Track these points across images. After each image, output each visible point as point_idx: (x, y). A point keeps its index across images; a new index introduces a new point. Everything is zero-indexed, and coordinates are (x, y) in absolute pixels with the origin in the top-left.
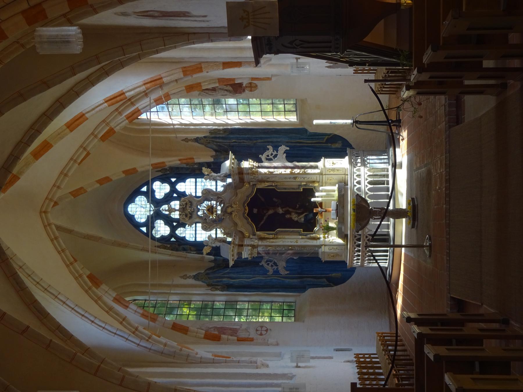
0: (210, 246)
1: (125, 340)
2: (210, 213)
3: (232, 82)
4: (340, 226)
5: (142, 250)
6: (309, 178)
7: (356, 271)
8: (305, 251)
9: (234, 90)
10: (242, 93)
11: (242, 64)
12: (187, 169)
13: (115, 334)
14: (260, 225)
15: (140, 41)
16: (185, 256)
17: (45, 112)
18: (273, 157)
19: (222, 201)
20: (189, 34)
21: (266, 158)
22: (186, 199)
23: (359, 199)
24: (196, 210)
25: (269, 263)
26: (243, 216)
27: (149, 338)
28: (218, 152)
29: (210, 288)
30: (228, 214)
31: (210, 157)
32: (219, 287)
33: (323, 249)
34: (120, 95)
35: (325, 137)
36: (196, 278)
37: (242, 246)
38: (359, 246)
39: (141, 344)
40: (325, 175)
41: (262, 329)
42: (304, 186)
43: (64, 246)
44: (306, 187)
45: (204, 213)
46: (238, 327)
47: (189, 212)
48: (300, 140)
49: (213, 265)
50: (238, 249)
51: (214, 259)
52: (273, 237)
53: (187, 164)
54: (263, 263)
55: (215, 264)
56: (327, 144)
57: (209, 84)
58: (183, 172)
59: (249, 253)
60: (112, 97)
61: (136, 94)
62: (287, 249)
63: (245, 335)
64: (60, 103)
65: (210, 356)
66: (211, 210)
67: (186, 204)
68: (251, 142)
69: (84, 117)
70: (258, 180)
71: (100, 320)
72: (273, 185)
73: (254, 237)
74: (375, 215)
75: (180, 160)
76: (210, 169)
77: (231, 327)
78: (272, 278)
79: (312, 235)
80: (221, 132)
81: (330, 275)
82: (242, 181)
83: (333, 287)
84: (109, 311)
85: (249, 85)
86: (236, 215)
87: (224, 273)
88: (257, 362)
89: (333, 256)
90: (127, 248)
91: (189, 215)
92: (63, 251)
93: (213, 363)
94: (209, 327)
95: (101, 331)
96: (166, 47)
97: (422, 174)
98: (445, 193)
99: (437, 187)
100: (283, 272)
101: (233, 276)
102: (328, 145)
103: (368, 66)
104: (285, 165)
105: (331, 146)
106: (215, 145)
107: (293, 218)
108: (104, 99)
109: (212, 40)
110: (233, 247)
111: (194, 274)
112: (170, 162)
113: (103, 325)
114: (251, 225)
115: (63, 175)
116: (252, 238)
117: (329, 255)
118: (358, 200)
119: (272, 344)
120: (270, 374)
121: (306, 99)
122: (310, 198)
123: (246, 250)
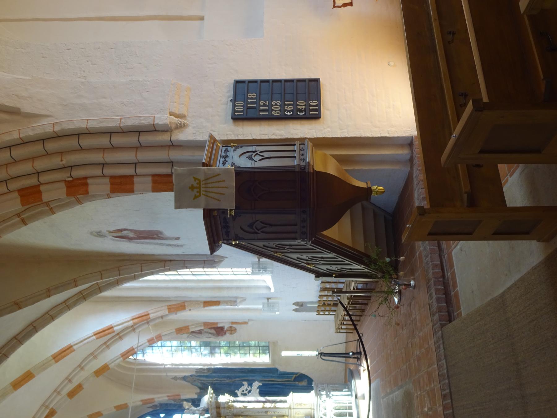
3: (215, 326)
6: (279, 412)
12: (175, 405)
20: (165, 261)
40: (293, 409)
53: (175, 400)
57: (196, 327)
60: (101, 331)
61: (124, 328)
64: (33, 326)
69: (71, 349)
70: (233, 414)
75: (168, 396)
80: (206, 371)
85: (230, 329)
96: (143, 272)
97: (395, 399)
98: (444, 413)
99: (426, 409)
103: (335, 278)
104: (257, 399)
105: (298, 384)
106: (199, 383)
108: (93, 333)
112: (159, 398)
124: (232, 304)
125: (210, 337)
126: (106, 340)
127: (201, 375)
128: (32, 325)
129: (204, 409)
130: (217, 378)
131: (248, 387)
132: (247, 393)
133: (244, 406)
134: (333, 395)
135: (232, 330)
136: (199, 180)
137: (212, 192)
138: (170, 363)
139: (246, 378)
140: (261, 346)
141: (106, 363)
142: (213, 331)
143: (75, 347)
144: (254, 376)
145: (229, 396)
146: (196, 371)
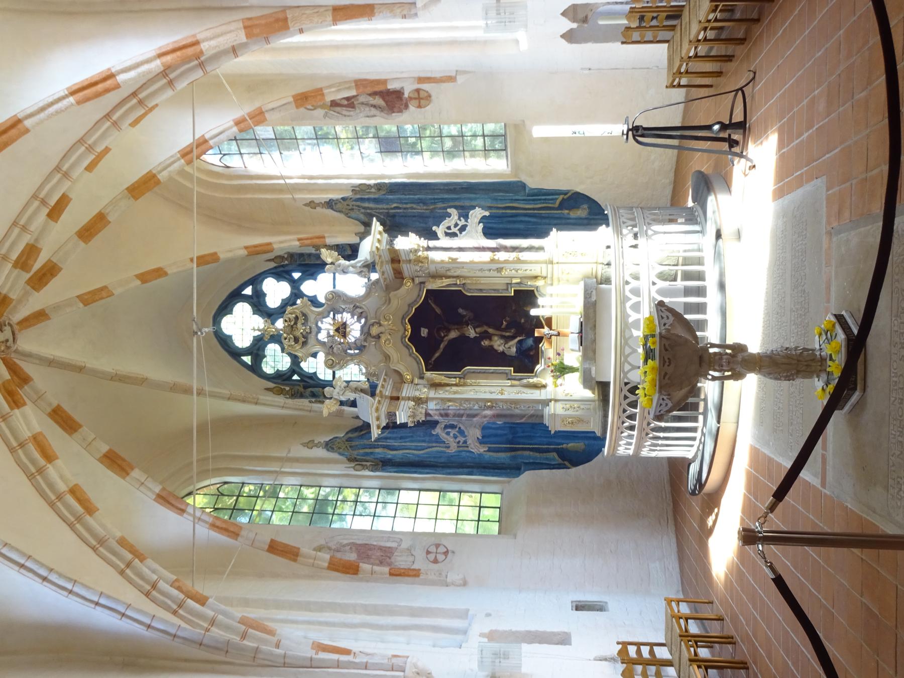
0: (336, 399)
3: (378, 88)
4: (587, 366)
5: (229, 399)
6: (526, 270)
8: (517, 411)
9: (387, 105)
10: (404, 111)
11: (376, 10)
13: (97, 604)
14: (433, 359)
16: (309, 409)
18: (459, 230)
19: (361, 313)
22: (295, 308)
23: (668, 318)
24: (314, 330)
26: (402, 343)
27: (180, 606)
29: (353, 465)
30: (374, 337)
32: (368, 464)
33: (552, 409)
34: (105, 79)
35: (557, 197)
37: (397, 398)
38: (632, 417)
40: (558, 263)
41: (437, 549)
42: (516, 285)
44: (520, 287)
45: (329, 336)
46: (394, 545)
47: (301, 333)
48: (512, 203)
52: (457, 381)
57: (339, 91)
58: (312, 263)
62: (483, 406)
63: (406, 561)
66: (342, 330)
67: (297, 318)
68: (425, 207)
69: (20, 126)
71: (60, 575)
72: (458, 283)
73: (421, 381)
74: (717, 368)
75: (299, 240)
77: (383, 544)
79: (531, 380)
80: (373, 190)
81: (564, 446)
82: (399, 275)
83: (569, 468)
84: (98, 546)
85: (416, 95)
86: (388, 339)
89: (572, 423)
91: (302, 340)
93: (311, 667)
94: (341, 543)
95: (64, 598)
102: (563, 212)
105: (569, 214)
106: (362, 213)
107: (496, 347)
108: (67, 89)
110: (379, 402)
111: (327, 439)
112: (281, 242)
113: (69, 586)
114: (415, 359)
116: (417, 384)
117: (563, 421)
118: (665, 320)
119: (453, 584)
121: (524, 121)
122: (528, 309)
123: (405, 408)
125: (375, 116)
126: (110, 109)
127: (363, 197)
129: (366, 264)
130: (397, 203)
132: (458, 232)
133: (450, 258)
134: (656, 233)
135: (421, 98)
138: (300, 174)
139: (457, 203)
140: (487, 136)
141: (150, 171)
142: (379, 101)
143: (28, 123)
144: (475, 199)
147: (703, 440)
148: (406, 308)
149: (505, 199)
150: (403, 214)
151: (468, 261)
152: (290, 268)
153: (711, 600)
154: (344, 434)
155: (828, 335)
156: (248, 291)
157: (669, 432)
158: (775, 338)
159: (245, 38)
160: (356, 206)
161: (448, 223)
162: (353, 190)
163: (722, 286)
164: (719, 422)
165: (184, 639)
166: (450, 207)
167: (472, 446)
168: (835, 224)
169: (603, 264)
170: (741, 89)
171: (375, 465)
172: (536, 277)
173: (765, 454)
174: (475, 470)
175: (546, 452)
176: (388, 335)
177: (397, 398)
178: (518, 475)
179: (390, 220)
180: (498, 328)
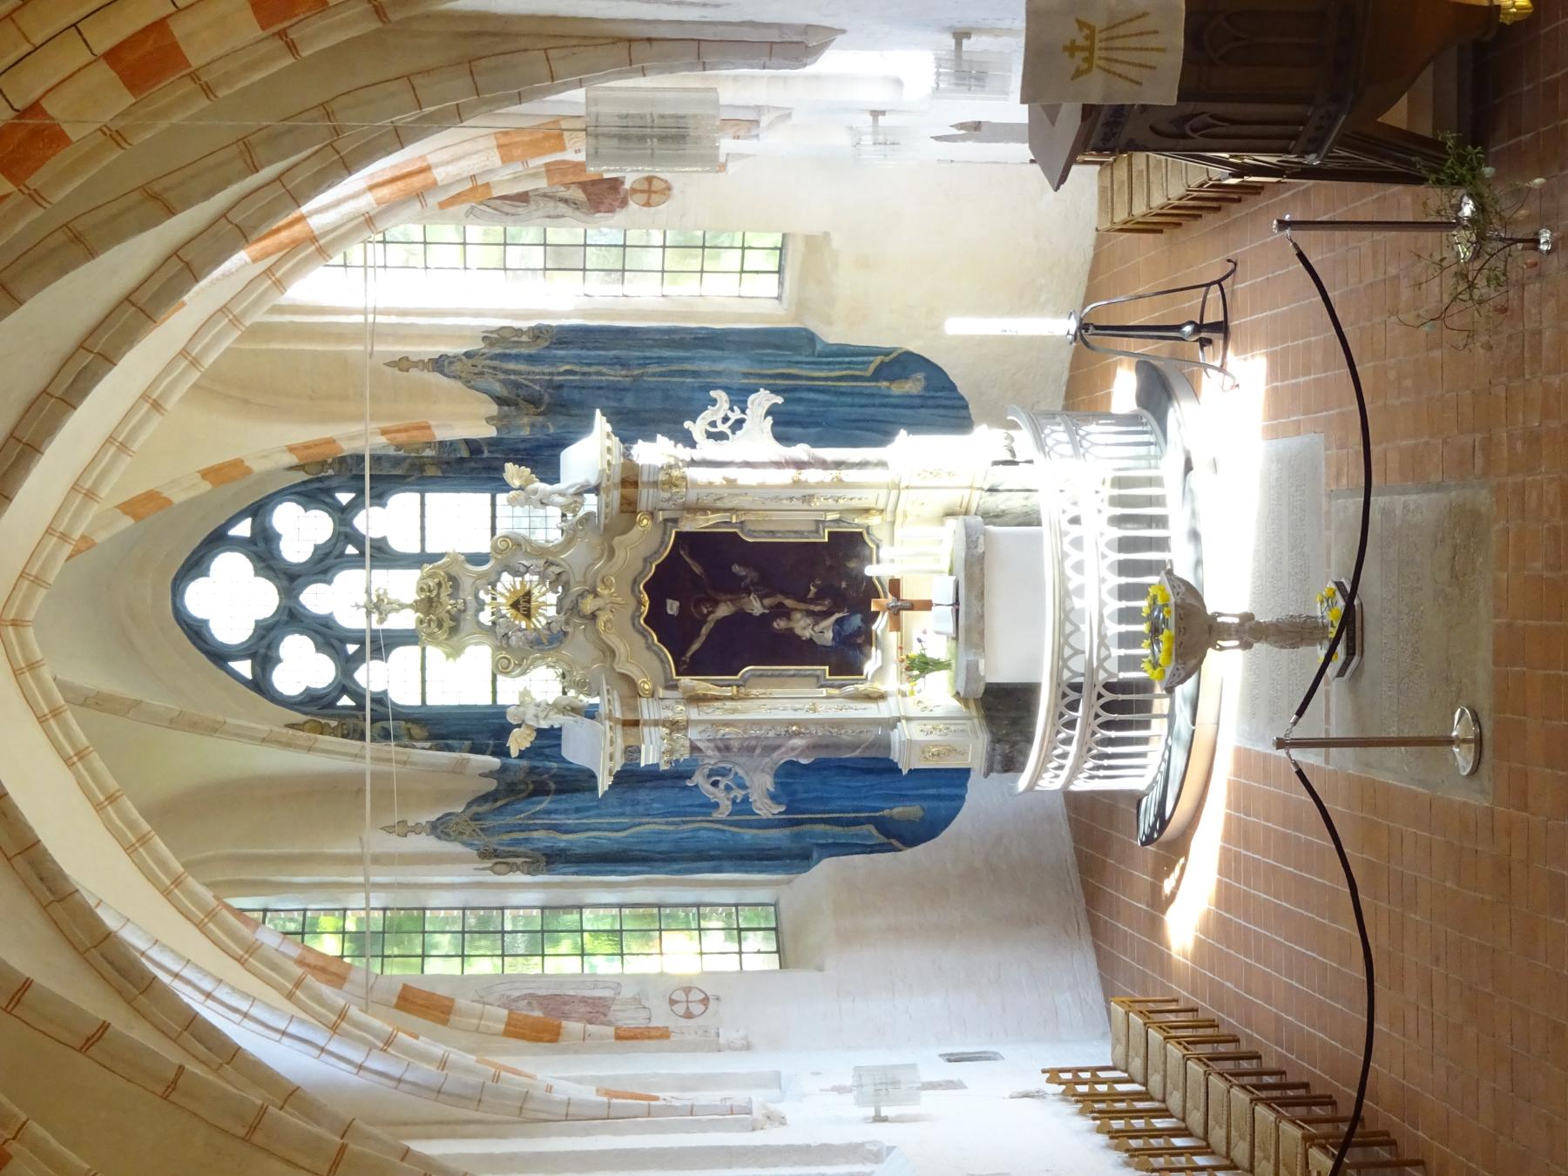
0: (529, 726)
1: (317, 1053)
2: (520, 616)
5: (263, 740)
6: (851, 499)
7: (967, 797)
9: (589, 200)
12: (397, 461)
13: (284, 1033)
14: (689, 654)
15: (470, 62)
17: (130, 294)
19: (559, 574)
21: (707, 432)
22: (438, 567)
25: (719, 778)
26: (634, 625)
28: (508, 405)
29: (490, 865)
30: (584, 617)
31: (484, 422)
32: (519, 861)
35: (871, 358)
36: (439, 831)
37: (636, 723)
39: (369, 1064)
40: (907, 488)
41: (687, 995)
42: (831, 524)
43: (83, 740)
46: (608, 993)
47: (448, 612)
48: (789, 367)
49: (491, 785)
50: (625, 734)
51: (499, 765)
52: (735, 692)
53: (399, 448)
54: (698, 779)
55: (499, 782)
56: (878, 381)
59: (663, 750)
62: (783, 733)
63: (634, 1018)
64: (182, 260)
65: (588, 1094)
66: (524, 604)
67: (439, 585)
68: (623, 373)
70: (684, 503)
72: (734, 521)
73: (669, 694)
75: (384, 432)
76: (529, 470)
77: (587, 993)
78: (697, 825)
80: (524, 338)
81: (886, 812)
82: (629, 507)
83: (900, 850)
84: (246, 956)
85: (646, 187)
87: (533, 814)
88: (751, 1109)
89: (939, 755)
90: (217, 735)
91: (448, 623)
92: (81, 755)
93: (608, 1118)
94: (508, 997)
100: (766, 809)
101: (563, 822)
102: (879, 384)
105: (889, 388)
106: (499, 380)
107: (798, 631)
109: (704, 63)
111: (433, 818)
112: (352, 438)
113: (244, 1006)
115: (81, 496)
117: (923, 752)
118: (1177, 590)
119: (731, 1047)
120: (808, 1146)
121: (827, 234)
124: (742, 133)
127: (508, 351)
128: (178, 257)
131: (731, 409)
132: (729, 432)
136: (1092, 29)
137: (1122, 62)
144: (722, 359)
145: (672, 443)
146: (484, 338)
147: (1166, 756)
148: (639, 565)
149: (776, 362)
150: (577, 384)
151: (755, 484)
152: (334, 483)
153: (1175, 997)
154: (464, 806)
155: (1329, 601)
156: (243, 529)
157: (1137, 729)
158: (1270, 607)
159: (261, 32)
160: (490, 367)
161: (712, 415)
162: (484, 338)
163: (1195, 536)
164: (1194, 723)
165: (415, 1084)
166: (715, 388)
167: (759, 804)
168: (1334, 487)
169: (982, 489)
170: (1219, 282)
171: (533, 863)
172: (867, 511)
173: (1259, 752)
174: (726, 864)
175: (854, 825)
176: (609, 613)
177: (636, 723)
178: (807, 868)
179: (550, 394)
180: (802, 598)
